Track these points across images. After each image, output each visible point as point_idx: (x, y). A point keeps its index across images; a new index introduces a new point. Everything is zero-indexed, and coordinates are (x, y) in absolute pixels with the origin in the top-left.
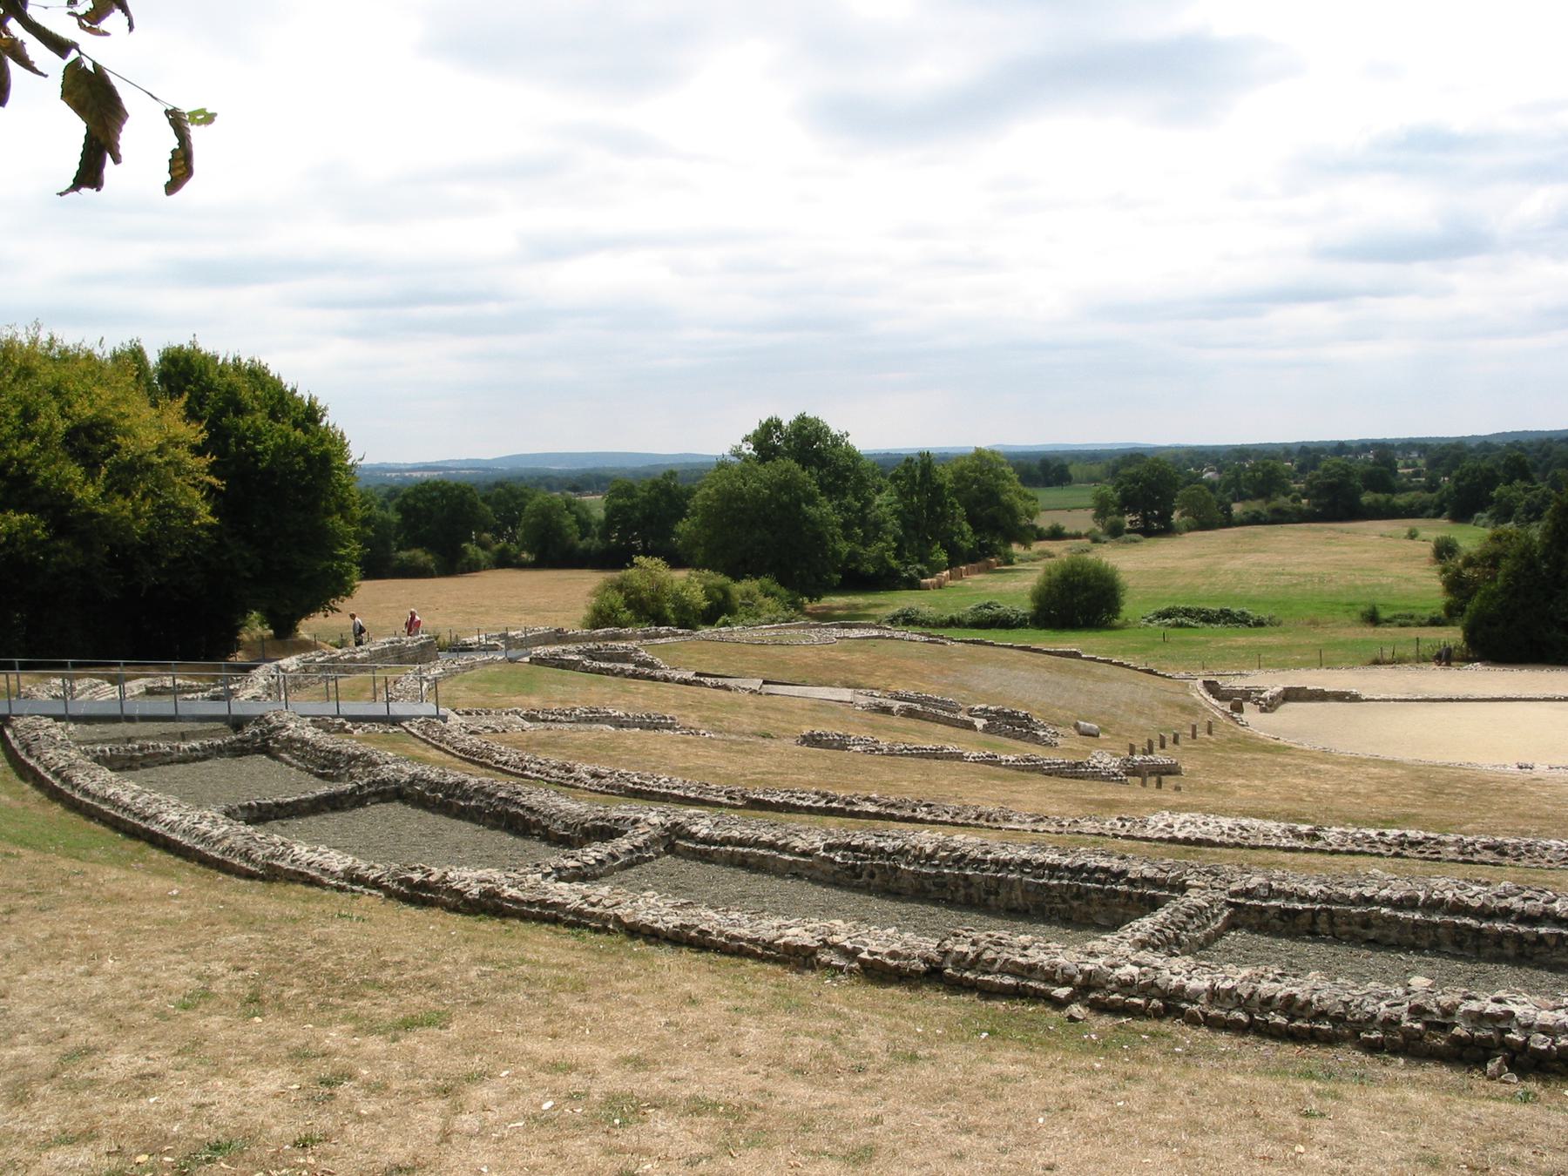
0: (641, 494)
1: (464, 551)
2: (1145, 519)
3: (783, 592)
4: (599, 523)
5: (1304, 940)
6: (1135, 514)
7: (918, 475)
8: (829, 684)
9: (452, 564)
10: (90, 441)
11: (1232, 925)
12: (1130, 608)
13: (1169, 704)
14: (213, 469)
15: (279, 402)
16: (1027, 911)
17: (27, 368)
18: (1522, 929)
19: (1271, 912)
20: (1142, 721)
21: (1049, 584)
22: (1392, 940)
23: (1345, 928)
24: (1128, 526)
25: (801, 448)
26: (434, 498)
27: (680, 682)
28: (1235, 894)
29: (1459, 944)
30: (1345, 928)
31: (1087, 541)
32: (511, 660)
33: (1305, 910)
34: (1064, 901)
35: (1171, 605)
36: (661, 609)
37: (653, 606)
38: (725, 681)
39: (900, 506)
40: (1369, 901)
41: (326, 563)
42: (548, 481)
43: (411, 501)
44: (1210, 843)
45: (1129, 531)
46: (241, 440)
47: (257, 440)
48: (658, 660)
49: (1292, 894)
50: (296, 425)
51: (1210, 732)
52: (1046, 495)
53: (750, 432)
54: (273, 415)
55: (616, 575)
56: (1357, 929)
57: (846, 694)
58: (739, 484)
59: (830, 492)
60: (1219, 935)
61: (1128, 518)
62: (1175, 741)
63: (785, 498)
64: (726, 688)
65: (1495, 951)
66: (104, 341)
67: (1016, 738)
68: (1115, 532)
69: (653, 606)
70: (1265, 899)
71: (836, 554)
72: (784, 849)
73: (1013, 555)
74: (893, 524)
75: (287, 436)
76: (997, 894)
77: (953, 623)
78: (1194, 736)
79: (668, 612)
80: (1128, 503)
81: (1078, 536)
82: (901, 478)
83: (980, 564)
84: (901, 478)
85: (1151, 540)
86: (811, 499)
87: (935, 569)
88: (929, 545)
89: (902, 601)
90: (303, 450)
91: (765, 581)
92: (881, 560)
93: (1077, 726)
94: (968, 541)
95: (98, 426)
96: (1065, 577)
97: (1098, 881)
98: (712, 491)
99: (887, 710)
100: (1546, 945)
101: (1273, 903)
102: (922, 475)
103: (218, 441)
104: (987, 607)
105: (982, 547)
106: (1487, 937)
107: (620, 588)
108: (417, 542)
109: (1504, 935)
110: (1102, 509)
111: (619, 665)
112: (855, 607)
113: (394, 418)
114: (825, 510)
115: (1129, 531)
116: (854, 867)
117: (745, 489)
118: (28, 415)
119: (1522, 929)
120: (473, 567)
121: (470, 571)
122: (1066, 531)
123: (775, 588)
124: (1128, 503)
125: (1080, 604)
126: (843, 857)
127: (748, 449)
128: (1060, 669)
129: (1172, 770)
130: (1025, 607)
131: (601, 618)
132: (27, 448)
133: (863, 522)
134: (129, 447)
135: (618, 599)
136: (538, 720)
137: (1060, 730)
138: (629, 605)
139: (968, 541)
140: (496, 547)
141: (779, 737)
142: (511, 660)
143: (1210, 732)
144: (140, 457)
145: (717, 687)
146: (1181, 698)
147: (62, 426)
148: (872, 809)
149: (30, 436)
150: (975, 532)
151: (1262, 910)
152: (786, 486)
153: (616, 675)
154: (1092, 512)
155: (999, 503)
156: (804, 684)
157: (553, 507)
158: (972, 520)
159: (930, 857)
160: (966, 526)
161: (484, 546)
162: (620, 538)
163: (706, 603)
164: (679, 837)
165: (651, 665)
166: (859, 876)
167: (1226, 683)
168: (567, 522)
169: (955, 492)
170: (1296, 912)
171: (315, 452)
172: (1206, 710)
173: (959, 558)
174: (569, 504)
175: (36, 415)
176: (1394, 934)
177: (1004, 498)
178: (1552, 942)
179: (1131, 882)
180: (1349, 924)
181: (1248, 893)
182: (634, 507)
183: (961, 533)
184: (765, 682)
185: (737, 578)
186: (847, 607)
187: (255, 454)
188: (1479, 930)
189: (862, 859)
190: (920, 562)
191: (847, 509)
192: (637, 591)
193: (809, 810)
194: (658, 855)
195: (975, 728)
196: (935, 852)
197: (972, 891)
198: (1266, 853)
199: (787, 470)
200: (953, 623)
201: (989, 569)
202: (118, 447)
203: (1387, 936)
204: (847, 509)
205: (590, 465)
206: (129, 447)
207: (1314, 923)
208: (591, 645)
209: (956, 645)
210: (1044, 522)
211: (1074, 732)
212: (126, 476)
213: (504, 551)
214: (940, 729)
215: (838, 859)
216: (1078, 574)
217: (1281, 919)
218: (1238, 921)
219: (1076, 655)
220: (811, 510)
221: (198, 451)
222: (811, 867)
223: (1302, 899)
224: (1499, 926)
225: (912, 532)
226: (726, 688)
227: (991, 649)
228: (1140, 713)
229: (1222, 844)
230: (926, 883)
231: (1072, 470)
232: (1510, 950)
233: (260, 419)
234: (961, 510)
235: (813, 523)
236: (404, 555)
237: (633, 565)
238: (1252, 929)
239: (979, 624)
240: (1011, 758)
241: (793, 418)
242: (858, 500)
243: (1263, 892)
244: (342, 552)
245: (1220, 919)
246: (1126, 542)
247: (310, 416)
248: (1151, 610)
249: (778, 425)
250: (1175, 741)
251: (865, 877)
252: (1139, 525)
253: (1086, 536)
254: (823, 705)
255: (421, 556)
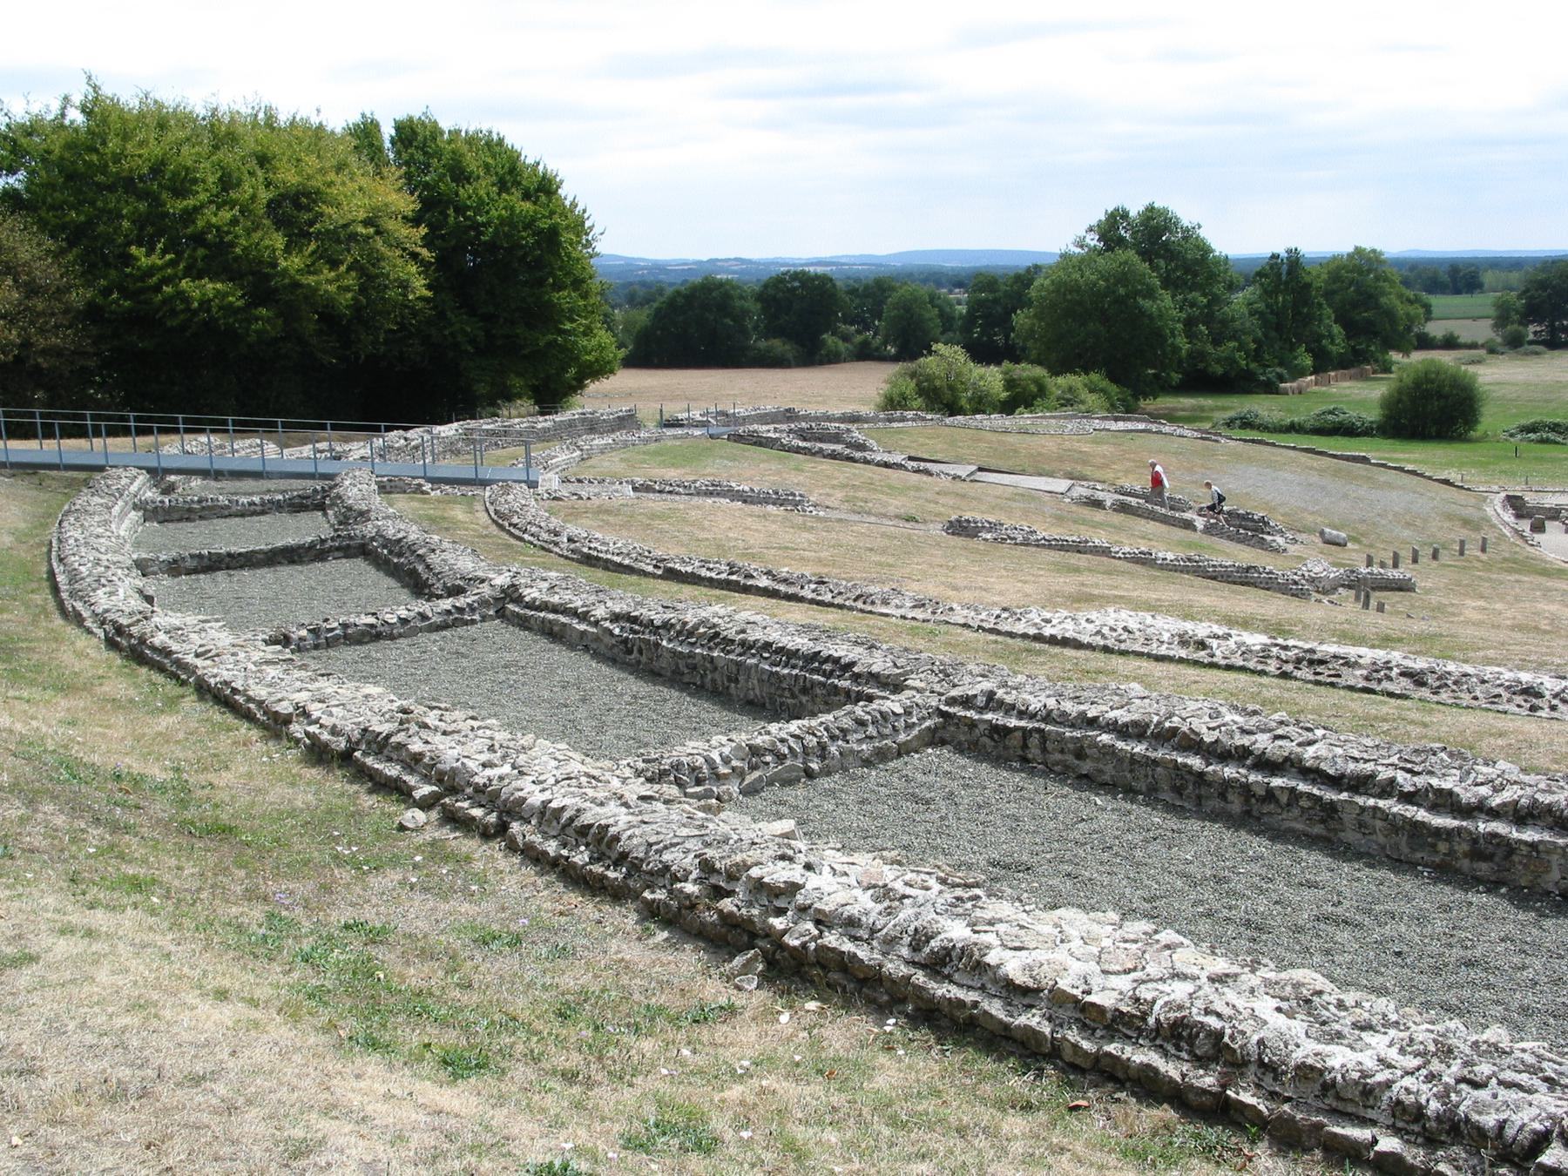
0: (1003, 288)
1: (823, 343)
2: (1553, 331)
3: (1113, 389)
4: (961, 317)
5: (1011, 769)
6: (1540, 324)
7: (1285, 278)
8: (1051, 474)
9: (811, 355)
10: (294, 210)
11: (934, 738)
12: (1489, 420)
13: (1449, 517)
14: (428, 242)
15: (509, 171)
16: (763, 705)
17: (232, 133)
18: (1253, 777)
19: (982, 727)
20: (1406, 533)
21: (1400, 391)
22: (1107, 778)
23: (1058, 756)
24: (1531, 337)
25: (1149, 247)
26: (795, 289)
27: (878, 464)
28: (952, 701)
29: (1178, 791)
30: (1058, 756)
31: (1482, 352)
32: (711, 436)
33: (1016, 728)
34: (793, 696)
35: (1538, 419)
36: (956, 399)
37: (948, 395)
38: (929, 465)
39: (1260, 306)
40: (1092, 722)
41: (550, 337)
42: (906, 276)
43: (771, 291)
44: (1077, 645)
45: (1531, 343)
46: (460, 210)
47: (478, 211)
48: (872, 443)
49: (1013, 707)
50: (527, 196)
51: (1483, 550)
52: (1438, 302)
53: (1094, 222)
54: (503, 186)
55: (912, 366)
56: (1070, 758)
57: (1061, 485)
58: (1077, 276)
59: (1177, 287)
60: (903, 751)
61: (1532, 328)
62: (1435, 556)
63: (1122, 291)
64: (928, 473)
65: (1216, 803)
66: (338, 118)
67: (1240, 541)
68: (1515, 343)
69: (948, 395)
70: (981, 710)
71: (1176, 349)
72: (584, 617)
73: (1392, 363)
74: (1252, 323)
75: (512, 209)
76: (737, 681)
77: (1293, 428)
78: (1462, 553)
79: (963, 402)
80: (1532, 312)
81: (1473, 346)
82: (1266, 276)
83: (1352, 371)
84: (1266, 276)
85: (1556, 353)
86: (1150, 293)
87: (1300, 372)
88: (1292, 348)
89: (1262, 407)
90: (530, 224)
91: (1095, 377)
92: (1231, 361)
93: (1322, 533)
94: (1338, 344)
95: (307, 195)
96: (1417, 384)
97: (824, 674)
98: (1047, 282)
99: (1098, 504)
100: (1277, 801)
101: (989, 716)
102: (1289, 273)
103: (432, 208)
104: (1331, 412)
105: (1355, 352)
106: (1209, 785)
107: (913, 375)
108: (772, 331)
109: (1227, 784)
110: (1502, 317)
111: (819, 445)
112: (1202, 409)
113: (652, 198)
114: (1166, 303)
115: (1531, 343)
116: (626, 640)
117: (1081, 281)
118: (227, 182)
119: (1253, 777)
120: (832, 359)
121: (830, 362)
122: (1462, 340)
123: (1105, 384)
124: (1532, 312)
125: (1436, 414)
126: (622, 629)
127: (1093, 240)
128: (1336, 473)
129: (1403, 587)
130: (1373, 415)
131: (893, 403)
132: (226, 215)
133: (1208, 319)
134: (332, 216)
135: (910, 386)
136: (654, 491)
137: (1300, 537)
138: (921, 392)
139: (1338, 344)
140: (859, 339)
141: (925, 522)
142: (711, 436)
143: (1483, 550)
144: (345, 226)
145: (918, 471)
146: (1470, 512)
147: (264, 196)
148: (764, 582)
149: (232, 204)
150: (1348, 337)
151: (972, 724)
152: (1123, 278)
153: (814, 454)
154: (1491, 322)
155: (1377, 306)
156: (1022, 473)
157: (916, 300)
158: (1342, 319)
159: (691, 634)
160: (1337, 329)
161: (846, 338)
162: (982, 334)
163: (1005, 394)
164: (513, 601)
165: (861, 447)
166: (630, 652)
167: (1530, 499)
168: (927, 316)
169: (1329, 295)
170: (1006, 731)
171: (544, 224)
172: (1494, 526)
173: (1323, 363)
174: (933, 299)
175: (239, 183)
176: (1109, 771)
177: (1383, 300)
178: (1284, 799)
179: (856, 677)
180: (1062, 751)
181: (967, 702)
182: (996, 301)
183: (1331, 337)
184: (980, 469)
185: (1056, 372)
186: (1193, 409)
187: (476, 226)
188: (1201, 774)
189: (636, 632)
190: (1281, 364)
191: (1192, 305)
192: (929, 378)
193: (711, 583)
194: (484, 618)
195: (1194, 529)
196: (696, 627)
197: (717, 676)
198: (1145, 664)
199: (1126, 263)
200: (1293, 428)
201: (1363, 377)
202: (322, 215)
203: (1101, 771)
204: (1192, 305)
205: (983, 262)
206: (332, 216)
207: (1025, 746)
208: (804, 425)
209: (1232, 443)
210: (1435, 329)
211: (1318, 540)
212: (334, 245)
213: (865, 344)
214: (1152, 527)
215: (617, 631)
216: (1432, 382)
217: (992, 739)
218: (947, 736)
219: (1365, 460)
220: (1146, 304)
221: (415, 221)
222: (597, 639)
223: (1022, 714)
224: (1229, 772)
225: (1273, 334)
226: (928, 473)
227: (1268, 449)
228: (1408, 525)
229: (1090, 647)
230: (681, 664)
231: (1488, 278)
232: (1236, 806)
233: (484, 187)
234: (1328, 311)
235: (1150, 317)
236: (763, 344)
237: (930, 353)
238: (960, 749)
239: (1320, 431)
240: (1170, 556)
241: (1142, 209)
242: (1205, 295)
243: (981, 701)
244: (568, 326)
245: (915, 732)
246: (1526, 354)
247: (546, 187)
248: (1513, 426)
249: (1125, 215)
250: (1435, 556)
251: (635, 654)
252: (1544, 336)
253: (1483, 346)
254: (1029, 496)
255: (778, 345)
